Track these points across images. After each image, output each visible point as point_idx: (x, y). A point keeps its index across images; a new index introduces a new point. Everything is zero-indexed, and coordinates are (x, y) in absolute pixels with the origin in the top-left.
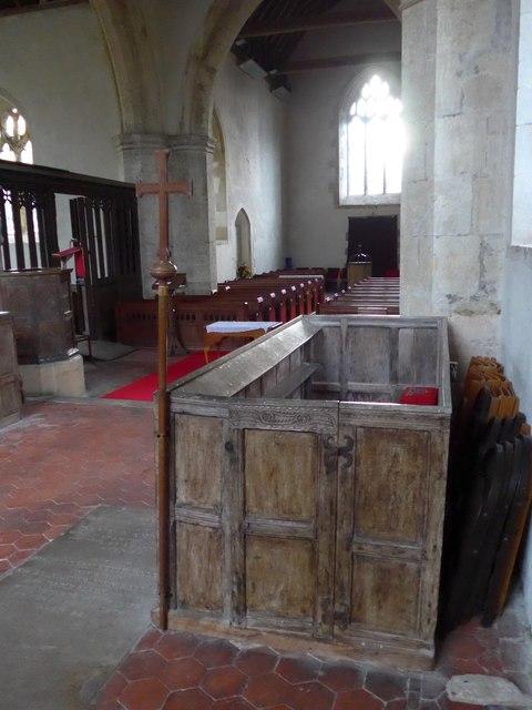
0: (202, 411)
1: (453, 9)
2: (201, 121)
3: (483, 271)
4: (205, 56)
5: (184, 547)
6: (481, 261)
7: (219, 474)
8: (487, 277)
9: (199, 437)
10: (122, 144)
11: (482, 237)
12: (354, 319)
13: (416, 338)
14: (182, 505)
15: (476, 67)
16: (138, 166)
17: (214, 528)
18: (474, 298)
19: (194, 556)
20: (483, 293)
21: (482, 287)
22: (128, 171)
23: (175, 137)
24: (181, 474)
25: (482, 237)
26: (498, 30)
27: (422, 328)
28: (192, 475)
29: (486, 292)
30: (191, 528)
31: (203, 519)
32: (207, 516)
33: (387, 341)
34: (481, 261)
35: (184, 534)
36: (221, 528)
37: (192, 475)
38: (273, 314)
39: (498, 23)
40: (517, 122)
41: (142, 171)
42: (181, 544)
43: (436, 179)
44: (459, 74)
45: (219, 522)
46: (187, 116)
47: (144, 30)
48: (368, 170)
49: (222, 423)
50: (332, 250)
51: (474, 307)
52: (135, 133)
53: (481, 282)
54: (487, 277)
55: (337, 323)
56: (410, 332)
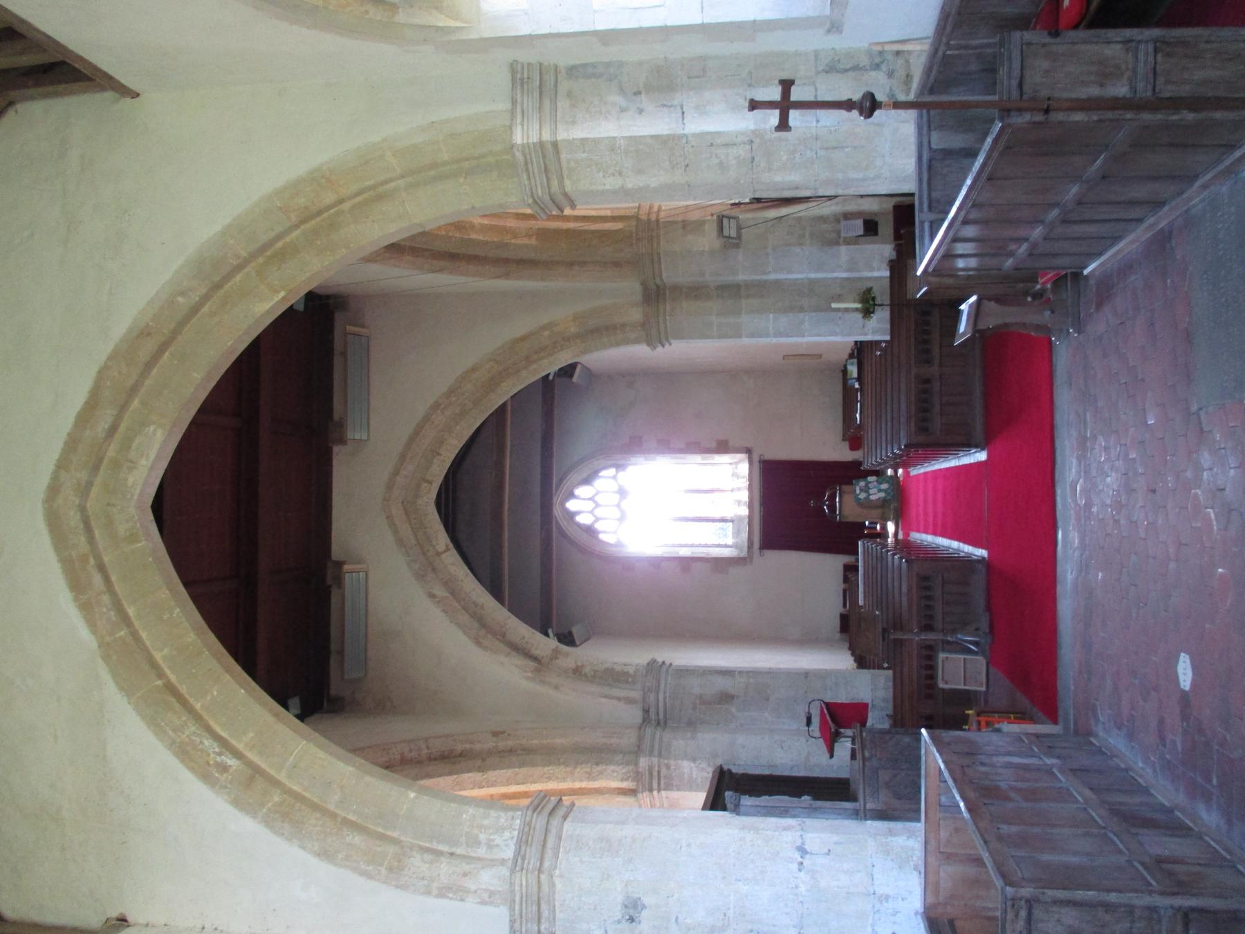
0: (1016, 65)
1: (574, 123)
2: (626, 674)
3: (856, 68)
4: (535, 659)
5: (1188, 87)
6: (846, 71)
7: (1088, 47)
8: (865, 61)
9: (1047, 71)
10: (651, 790)
11: (818, 73)
12: (921, 204)
13: (941, 127)
14: (1134, 90)
15: (635, 94)
16: (686, 765)
17: (1156, 51)
18: (890, 74)
19: (1199, 75)
20: (884, 67)
21: (877, 67)
22: (692, 786)
23: (646, 711)
24: (1094, 91)
25: (818, 73)
26: (600, 75)
27: (929, 121)
28: (1093, 78)
29: (882, 62)
30: (1161, 80)
31: (1146, 62)
32: (1141, 57)
33: (947, 162)
34: (846, 71)
35: (1170, 87)
36: (1156, 41)
37: (1093, 78)
38: (922, 528)
39: (594, 75)
40: (699, 22)
41: (694, 760)
42: (1185, 90)
43: (752, 127)
44: (641, 111)
45: (1147, 42)
46: (616, 692)
47: (495, 734)
48: (695, 487)
49: (1029, 44)
50: (818, 573)
51: (901, 73)
52: (636, 764)
53: (872, 69)
54: (865, 61)
55: (927, 226)
56: (935, 136)
